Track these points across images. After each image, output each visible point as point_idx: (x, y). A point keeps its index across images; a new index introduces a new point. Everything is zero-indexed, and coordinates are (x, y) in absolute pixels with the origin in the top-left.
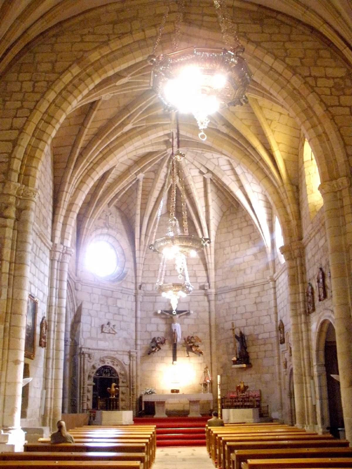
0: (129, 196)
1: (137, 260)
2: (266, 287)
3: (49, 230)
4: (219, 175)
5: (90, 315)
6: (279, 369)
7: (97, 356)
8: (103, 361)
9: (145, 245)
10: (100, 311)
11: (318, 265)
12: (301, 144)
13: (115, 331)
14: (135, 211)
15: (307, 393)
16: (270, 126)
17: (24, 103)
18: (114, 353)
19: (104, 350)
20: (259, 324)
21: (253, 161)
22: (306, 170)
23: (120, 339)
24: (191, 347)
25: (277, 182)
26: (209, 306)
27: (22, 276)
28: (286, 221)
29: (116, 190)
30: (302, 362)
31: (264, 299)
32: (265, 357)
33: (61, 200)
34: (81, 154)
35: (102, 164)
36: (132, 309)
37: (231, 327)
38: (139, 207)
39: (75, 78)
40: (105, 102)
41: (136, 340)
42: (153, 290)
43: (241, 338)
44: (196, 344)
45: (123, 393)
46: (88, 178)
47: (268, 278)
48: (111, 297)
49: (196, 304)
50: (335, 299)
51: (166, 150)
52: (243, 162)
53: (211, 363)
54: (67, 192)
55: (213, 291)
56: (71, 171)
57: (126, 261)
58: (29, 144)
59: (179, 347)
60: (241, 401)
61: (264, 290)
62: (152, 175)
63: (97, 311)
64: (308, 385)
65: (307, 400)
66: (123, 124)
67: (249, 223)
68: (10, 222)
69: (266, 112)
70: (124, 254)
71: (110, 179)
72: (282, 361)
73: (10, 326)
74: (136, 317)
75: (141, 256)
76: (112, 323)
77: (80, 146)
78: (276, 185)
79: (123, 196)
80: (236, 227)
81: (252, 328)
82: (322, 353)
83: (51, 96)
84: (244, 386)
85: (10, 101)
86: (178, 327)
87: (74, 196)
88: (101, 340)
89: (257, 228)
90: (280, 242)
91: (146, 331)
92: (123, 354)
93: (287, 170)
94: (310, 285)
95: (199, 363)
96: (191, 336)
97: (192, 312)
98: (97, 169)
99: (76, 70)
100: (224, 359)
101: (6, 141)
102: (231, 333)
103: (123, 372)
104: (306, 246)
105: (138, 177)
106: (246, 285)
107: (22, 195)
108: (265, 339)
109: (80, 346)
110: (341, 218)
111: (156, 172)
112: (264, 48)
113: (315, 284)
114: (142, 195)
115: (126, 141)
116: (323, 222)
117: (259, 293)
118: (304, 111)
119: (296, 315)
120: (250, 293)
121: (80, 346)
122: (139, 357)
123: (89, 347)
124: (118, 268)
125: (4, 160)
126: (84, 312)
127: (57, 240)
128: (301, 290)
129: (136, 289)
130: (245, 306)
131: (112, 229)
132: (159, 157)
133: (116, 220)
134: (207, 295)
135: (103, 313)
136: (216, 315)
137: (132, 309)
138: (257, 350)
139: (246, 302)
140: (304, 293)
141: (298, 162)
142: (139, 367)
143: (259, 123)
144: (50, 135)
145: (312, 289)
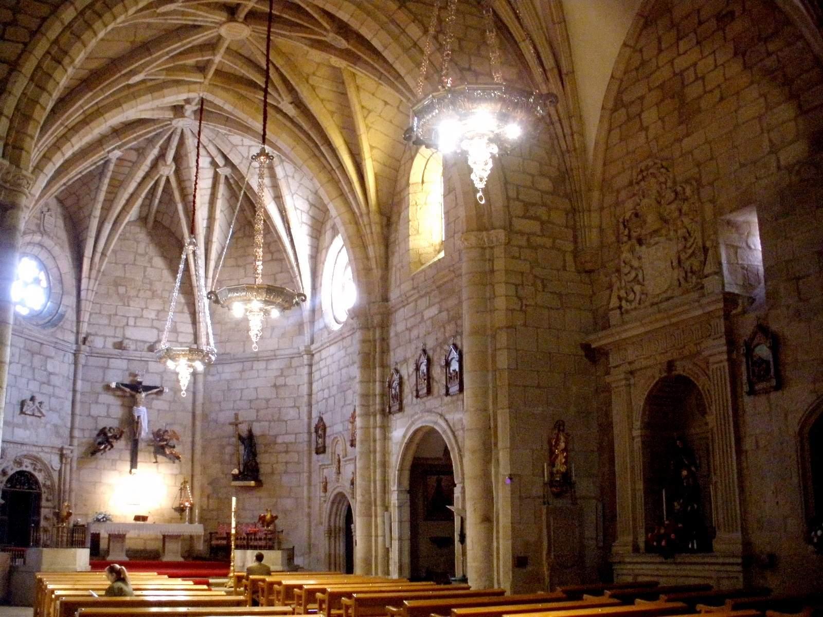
0: (84, 184)
1: (83, 293)
2: (295, 362)
8: (20, 464)
9: (99, 271)
10: (21, 376)
12: (407, 155)
13: (41, 412)
16: (365, 118)
17: (20, 17)
19: (22, 444)
20: (279, 420)
23: (48, 426)
24: (163, 447)
25: (359, 208)
28: (364, 269)
30: (372, 484)
31: (290, 381)
32: (286, 472)
36: (68, 377)
38: (99, 206)
42: (104, 347)
43: (249, 441)
44: (172, 443)
45: (46, 518)
47: (302, 348)
48: (39, 354)
52: (308, 166)
53: (192, 476)
58: (24, 94)
59: (141, 445)
60: (265, 539)
61: (291, 367)
62: (133, 156)
64: (379, 520)
65: (376, 541)
66: (133, 73)
67: (276, 256)
69: (364, 95)
70: (61, 282)
72: (317, 480)
74: (74, 391)
76: (39, 398)
82: (407, 474)
84: (272, 517)
86: (142, 412)
88: (19, 426)
89: (292, 268)
91: (89, 415)
92: (51, 453)
93: (377, 191)
95: (172, 474)
96: (163, 429)
97: (166, 390)
98: (74, 140)
100: (215, 469)
102: (230, 429)
103: (48, 483)
104: (396, 311)
105: (110, 155)
108: (287, 444)
110: (488, 288)
111: (141, 152)
112: (410, 11)
113: (407, 371)
114: (109, 185)
115: (127, 99)
120: (266, 369)
122: (75, 459)
124: (49, 304)
129: (77, 343)
130: (256, 389)
131: (49, 236)
132: (155, 130)
133: (56, 222)
135: (24, 380)
136: (204, 398)
137: (68, 377)
138: (273, 459)
139: (259, 381)
140: (383, 382)
141: (396, 181)
142: (74, 476)
143: (351, 112)
144: (58, 83)
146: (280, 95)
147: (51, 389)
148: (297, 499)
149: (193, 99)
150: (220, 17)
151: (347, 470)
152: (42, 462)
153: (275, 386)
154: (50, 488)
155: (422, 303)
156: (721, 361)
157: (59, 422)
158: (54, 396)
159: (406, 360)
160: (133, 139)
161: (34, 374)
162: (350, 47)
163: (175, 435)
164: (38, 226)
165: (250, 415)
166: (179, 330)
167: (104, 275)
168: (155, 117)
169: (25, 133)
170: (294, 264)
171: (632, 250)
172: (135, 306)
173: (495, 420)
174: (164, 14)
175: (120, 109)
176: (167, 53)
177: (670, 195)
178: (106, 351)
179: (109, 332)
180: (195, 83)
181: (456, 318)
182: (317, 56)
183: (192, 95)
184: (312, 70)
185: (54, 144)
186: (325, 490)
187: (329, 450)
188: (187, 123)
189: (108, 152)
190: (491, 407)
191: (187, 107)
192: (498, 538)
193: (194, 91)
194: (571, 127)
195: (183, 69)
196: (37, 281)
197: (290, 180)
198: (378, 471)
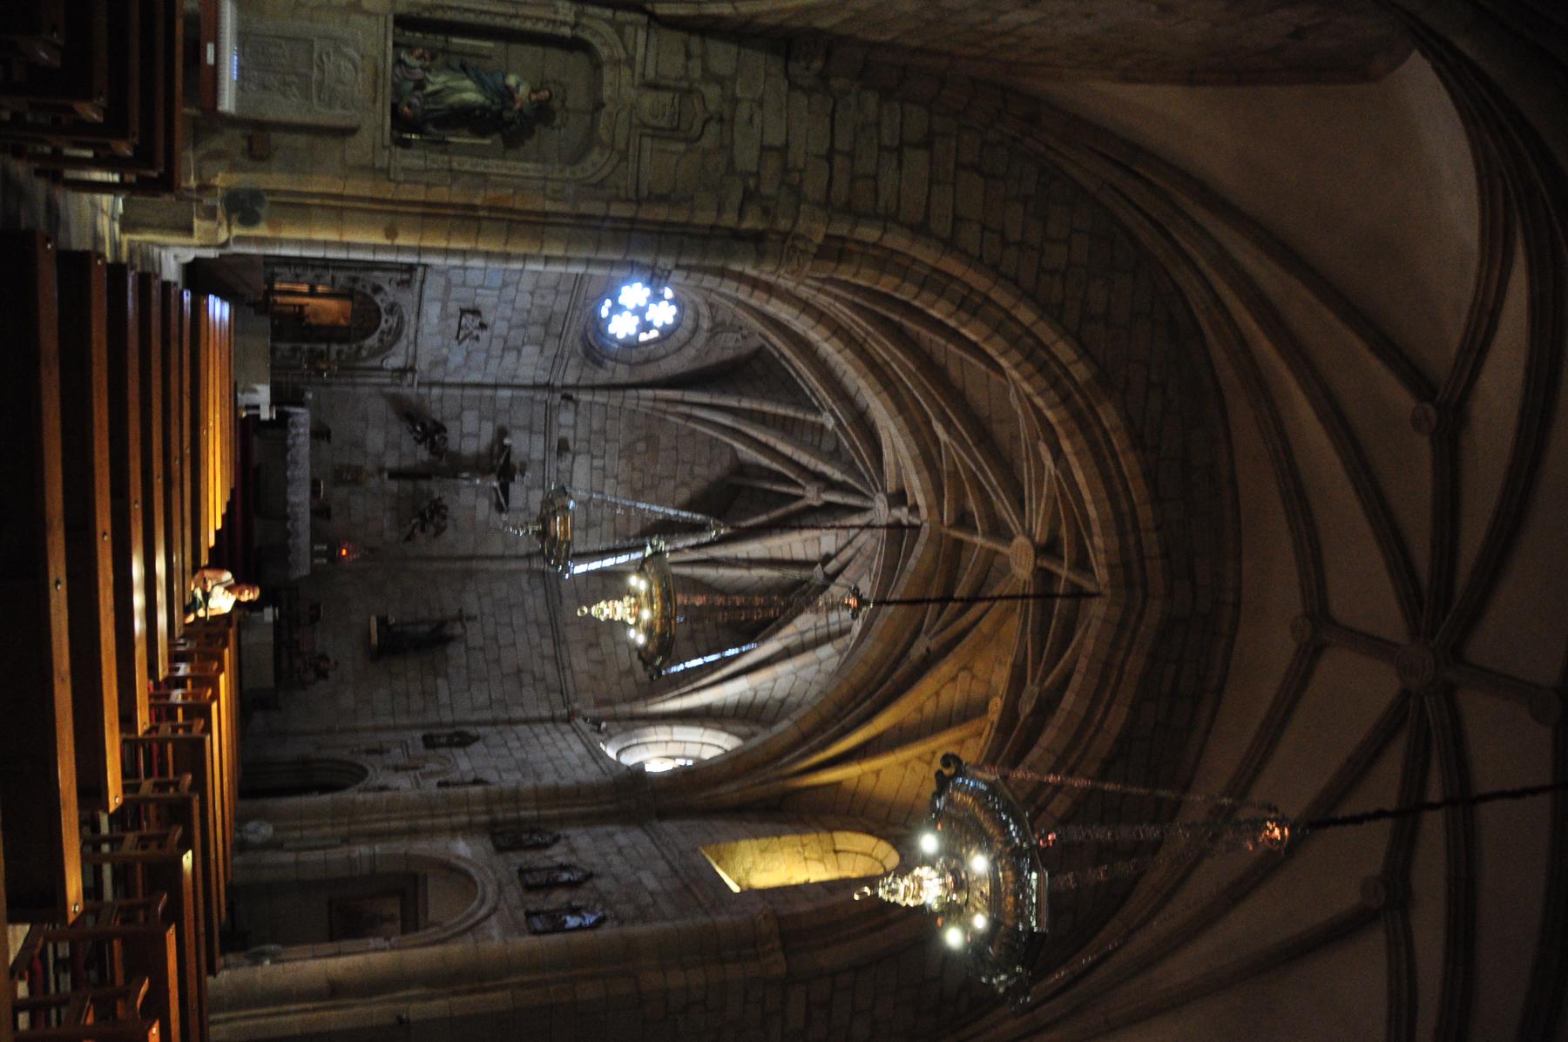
1: (633, 393)
5: (505, 285)
9: (665, 412)
14: (748, 396)
16: (919, 758)
18: (412, 336)
19: (418, 315)
22: (814, 836)
23: (445, 351)
26: (517, 557)
31: (528, 693)
35: (859, 363)
38: (755, 405)
42: (560, 426)
46: (828, 328)
47: (577, 706)
48: (546, 333)
51: (884, 490)
56: (850, 297)
57: (632, 365)
58: (914, 260)
62: (828, 445)
63: (513, 301)
65: (295, 828)
66: (948, 425)
68: (729, 219)
70: (647, 361)
74: (496, 386)
76: (484, 335)
78: (786, 759)
83: (1026, 315)
87: (788, 297)
88: (444, 308)
89: (691, 682)
91: (462, 409)
97: (504, 517)
99: (1081, 372)
101: (928, 207)
103: (364, 353)
104: (645, 831)
105: (826, 414)
106: (563, 647)
111: (835, 456)
113: (558, 854)
117: (543, 679)
120: (543, 657)
125: (881, 204)
128: (545, 812)
129: (564, 387)
131: (708, 340)
133: (729, 346)
135: (508, 313)
140: (539, 819)
146: (936, 634)
147: (496, 351)
149: (918, 516)
151: (403, 782)
153: (519, 671)
155: (662, 866)
157: (451, 366)
159: (573, 851)
160: (851, 442)
161: (518, 327)
162: (1022, 718)
163: (440, 530)
164: (723, 323)
166: (591, 532)
167: (660, 420)
168: (887, 469)
170: (696, 685)
172: (620, 467)
174: (1037, 456)
176: (980, 468)
178: (554, 429)
179: (582, 431)
181: (642, 915)
182: (1001, 677)
183: (924, 512)
184: (980, 674)
185: (840, 327)
186: (370, 752)
187: (431, 752)
188: (881, 511)
189: (832, 411)
190: (514, 979)
191: (905, 510)
192: (306, 1011)
195: (960, 497)
196: (646, 326)
197: (816, 667)
198: (404, 824)
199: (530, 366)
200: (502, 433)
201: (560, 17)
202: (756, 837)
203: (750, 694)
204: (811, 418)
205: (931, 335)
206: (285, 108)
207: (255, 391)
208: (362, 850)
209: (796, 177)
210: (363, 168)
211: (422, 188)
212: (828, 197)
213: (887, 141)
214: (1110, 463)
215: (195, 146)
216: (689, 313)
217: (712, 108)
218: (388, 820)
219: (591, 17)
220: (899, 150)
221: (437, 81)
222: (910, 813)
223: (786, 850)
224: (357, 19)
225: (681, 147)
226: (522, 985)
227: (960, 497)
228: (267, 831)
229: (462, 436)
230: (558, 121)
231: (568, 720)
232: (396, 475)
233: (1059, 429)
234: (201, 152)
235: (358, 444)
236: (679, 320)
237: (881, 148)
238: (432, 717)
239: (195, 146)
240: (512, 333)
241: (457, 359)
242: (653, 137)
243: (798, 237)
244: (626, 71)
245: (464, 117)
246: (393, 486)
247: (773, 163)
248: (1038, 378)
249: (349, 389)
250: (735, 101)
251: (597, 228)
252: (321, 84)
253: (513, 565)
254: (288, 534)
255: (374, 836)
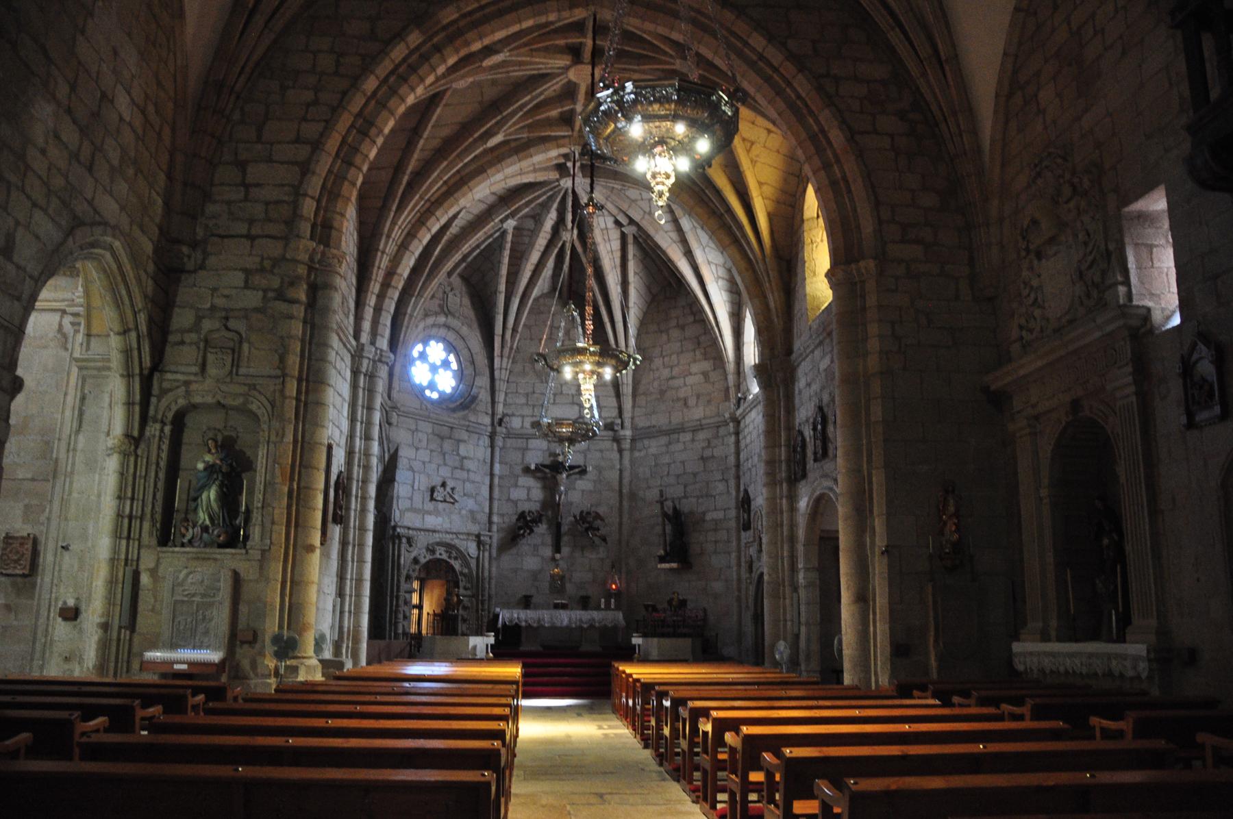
1: (497, 373)
2: (722, 431)
3: (352, 318)
4: (651, 231)
5: (411, 469)
6: (739, 574)
7: (422, 540)
8: (433, 552)
9: (511, 348)
11: (815, 401)
15: (785, 614)
16: (748, 151)
19: (434, 531)
21: (714, 213)
23: (464, 512)
27: (320, 404)
29: (465, 248)
31: (717, 452)
32: (715, 552)
33: (373, 266)
34: (410, 185)
35: (446, 205)
37: (657, 497)
38: (503, 281)
39: (412, 52)
40: (456, 91)
41: (491, 514)
47: (727, 415)
49: (598, 455)
50: (840, 461)
51: (558, 180)
54: (383, 252)
55: (628, 433)
56: (392, 214)
58: (330, 171)
62: (530, 224)
63: (424, 463)
64: (788, 601)
65: (785, 626)
68: (299, 311)
70: (473, 363)
71: (454, 230)
73: (298, 488)
74: (492, 475)
75: (504, 366)
76: (450, 484)
77: (410, 169)
79: (475, 258)
80: (673, 323)
81: (694, 500)
83: (370, 84)
85: (294, 88)
87: (396, 260)
88: (429, 513)
90: (751, 355)
91: (509, 500)
94: (801, 433)
97: (590, 469)
98: (438, 213)
99: (414, 38)
102: (657, 509)
103: (466, 571)
107: (319, 262)
108: (716, 521)
109: (393, 523)
111: (537, 218)
113: (808, 433)
116: (828, 330)
118: (813, 138)
119: (772, 482)
120: (693, 440)
121: (393, 523)
122: (495, 545)
123: (410, 525)
125: (286, 198)
126: (402, 463)
127: (365, 338)
129: (493, 424)
130: (683, 462)
131: (454, 316)
132: (545, 193)
133: (460, 301)
134: (617, 440)
135: (434, 466)
140: (788, 446)
145: (804, 440)
147: (465, 475)
148: (726, 581)
150: (562, 61)
152: (458, 549)
154: (468, 576)
156: (1128, 396)
157: (476, 508)
158: (468, 480)
163: (598, 516)
164: (441, 306)
165: (677, 491)
169: (334, 212)
171: (1031, 268)
173: (870, 482)
175: (485, 175)
176: (521, 108)
177: (1067, 191)
180: (564, 137)
189: (502, 221)
193: (563, 146)
194: (958, 126)
195: (549, 123)
196: (446, 364)
198: (786, 547)
199: (476, 450)
200: (527, 470)
201: (157, 433)
202: (805, 279)
203: (721, 282)
204: (509, 238)
205: (418, 151)
206: (220, 618)
207: (475, 648)
208: (801, 577)
209: (267, 264)
210: (261, 568)
211: (276, 527)
212: (281, 238)
213: (242, 195)
214: (487, 11)
215: (247, 678)
216: (434, 331)
217: (217, 325)
218: (782, 558)
219: (156, 411)
220: (247, 186)
221: (203, 517)
222: (792, 158)
223: (815, 256)
224: (161, 572)
225: (245, 346)
226: (869, 461)
227: (549, 123)
228: (781, 645)
229: (529, 499)
230: (234, 434)
231: (737, 422)
232: (557, 549)
233: (463, 53)
234: (252, 675)
235: (535, 575)
236: (440, 339)
237: (246, 199)
238: (733, 524)
239: (247, 678)
240: (450, 463)
241: (470, 504)
242: (238, 366)
243: (311, 259)
244: (194, 387)
245: (229, 499)
246: (565, 550)
247: (257, 280)
248: (421, 72)
249: (493, 582)
250: (213, 308)
251: (306, 404)
252: (203, 596)
253: (626, 462)
254: (592, 626)
255: (793, 569)
